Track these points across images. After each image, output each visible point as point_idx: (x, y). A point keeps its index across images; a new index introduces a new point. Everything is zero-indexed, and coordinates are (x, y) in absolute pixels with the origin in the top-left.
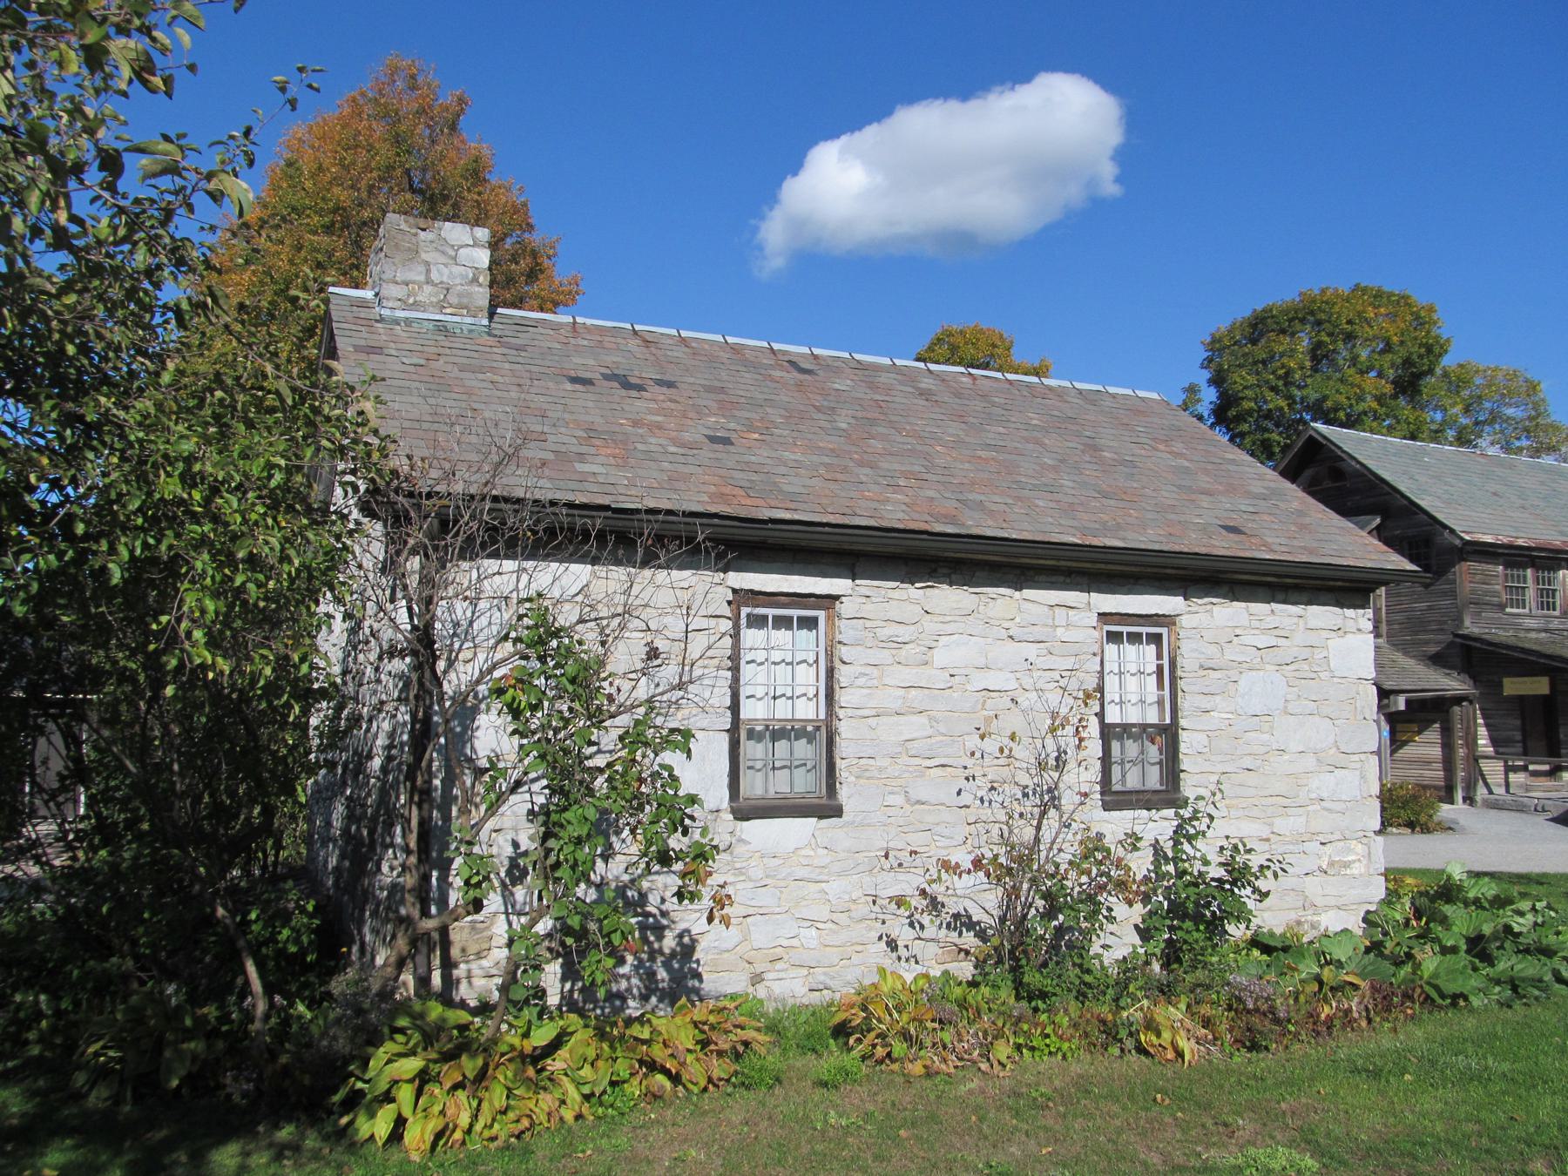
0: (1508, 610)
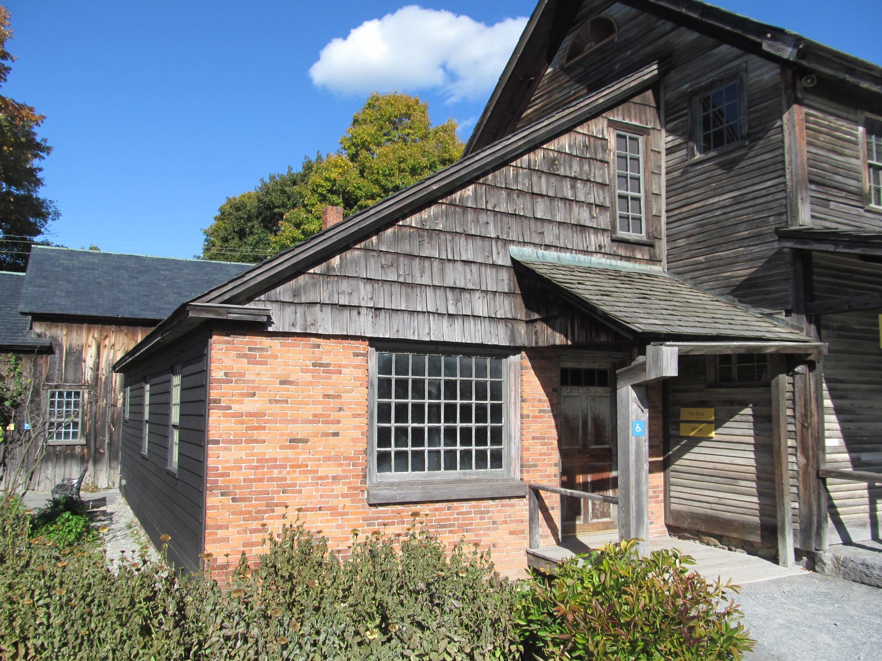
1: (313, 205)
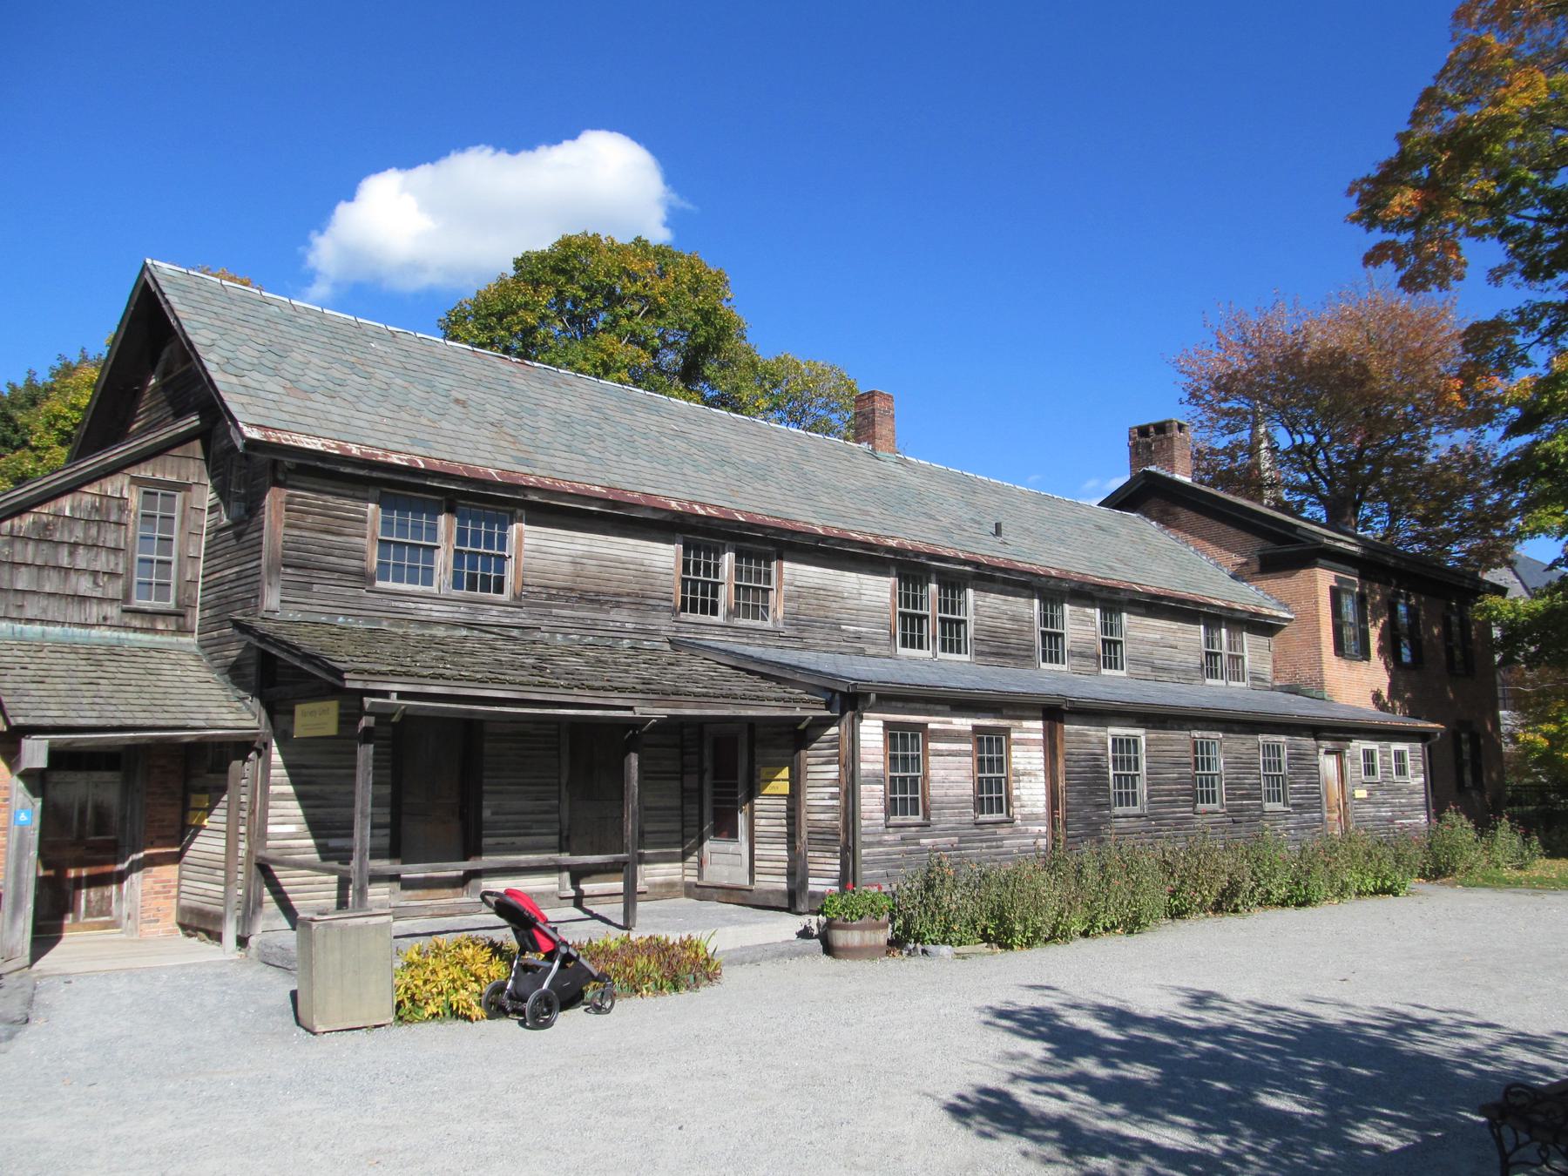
0: (379, 584)
1: (48, 448)
